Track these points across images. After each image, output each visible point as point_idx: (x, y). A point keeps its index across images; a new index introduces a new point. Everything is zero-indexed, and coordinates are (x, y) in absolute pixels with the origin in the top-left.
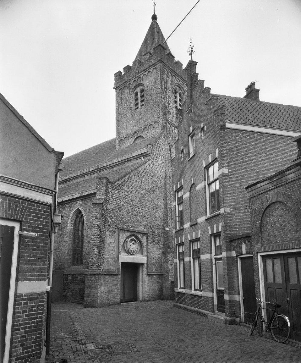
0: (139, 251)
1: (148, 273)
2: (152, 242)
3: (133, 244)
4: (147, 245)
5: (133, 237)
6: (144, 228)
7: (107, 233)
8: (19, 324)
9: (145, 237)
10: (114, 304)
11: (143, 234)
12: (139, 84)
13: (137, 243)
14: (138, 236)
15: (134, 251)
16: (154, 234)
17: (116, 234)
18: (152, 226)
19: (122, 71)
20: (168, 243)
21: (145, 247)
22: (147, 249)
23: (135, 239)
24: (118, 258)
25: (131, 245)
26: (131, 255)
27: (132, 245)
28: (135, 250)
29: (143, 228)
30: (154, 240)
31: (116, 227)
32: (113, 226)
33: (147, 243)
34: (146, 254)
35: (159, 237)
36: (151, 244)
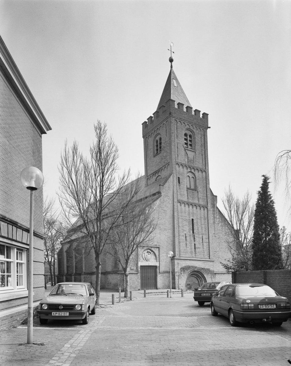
12: (158, 133)
19: (147, 121)
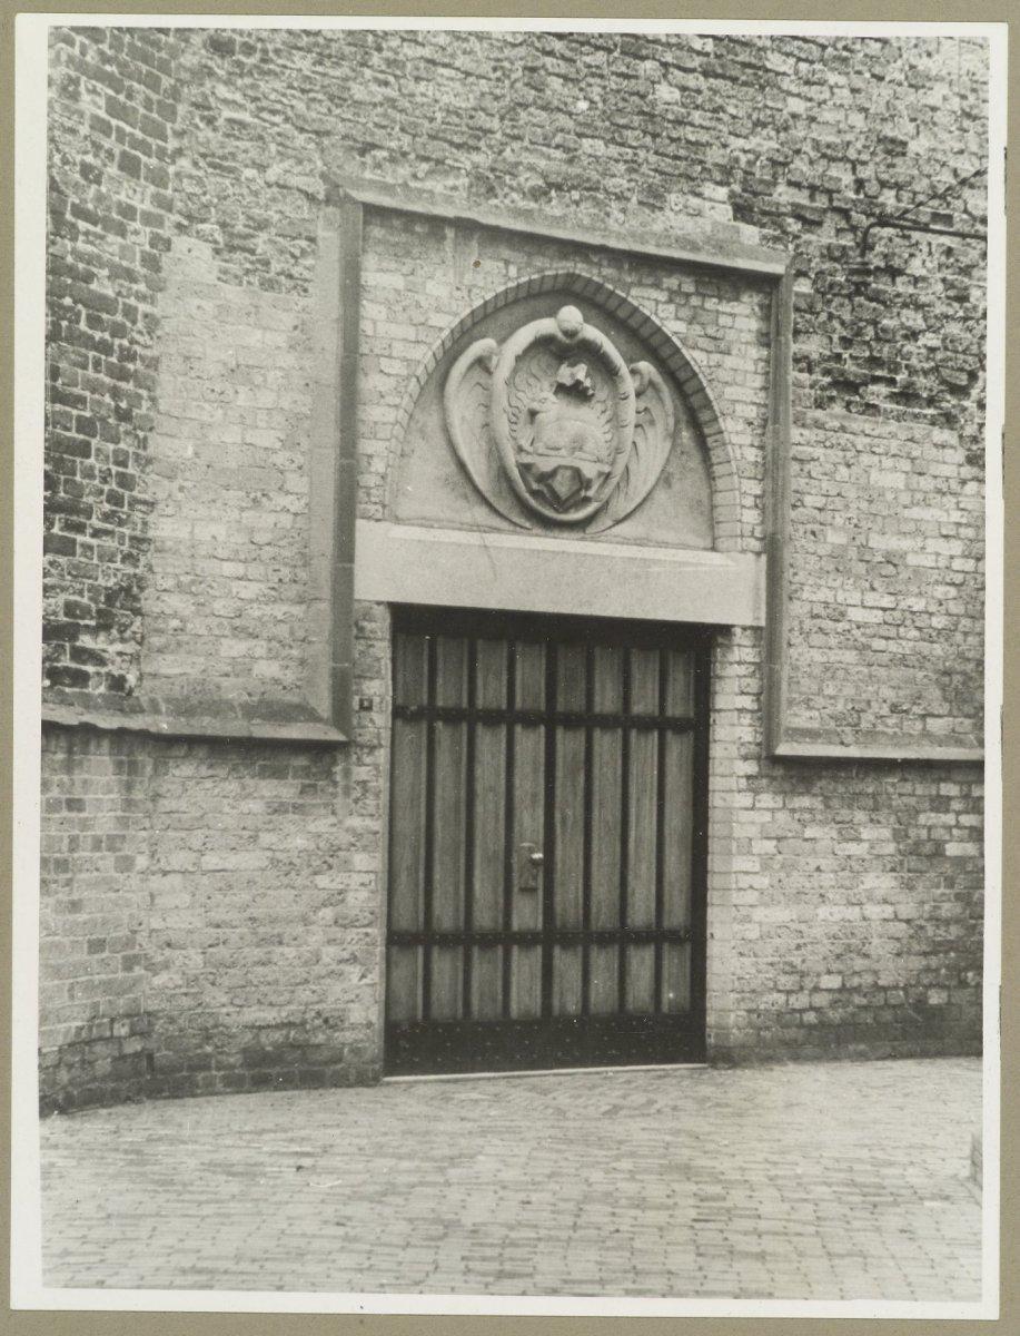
0: (665, 479)
1: (784, 749)
2: (848, 386)
3: (576, 393)
4: (771, 421)
5: (571, 315)
6: (742, 211)
7: (193, 258)
8: (103, 951)
9: (742, 317)
10: (288, 1065)
11: (724, 280)
13: (630, 385)
14: (653, 303)
15: (580, 481)
16: (880, 284)
17: (325, 270)
18: (860, 184)
20: (576, 555)
21: (738, 439)
22: (772, 467)
23: (592, 333)
24: (345, 550)
25: (533, 414)
26: (548, 524)
27: (555, 408)
28: (589, 471)
29: (725, 213)
30: (874, 361)
31: (320, 189)
32: (273, 174)
33: (774, 385)
34: (751, 517)
35: (954, 329)
36: (838, 408)
